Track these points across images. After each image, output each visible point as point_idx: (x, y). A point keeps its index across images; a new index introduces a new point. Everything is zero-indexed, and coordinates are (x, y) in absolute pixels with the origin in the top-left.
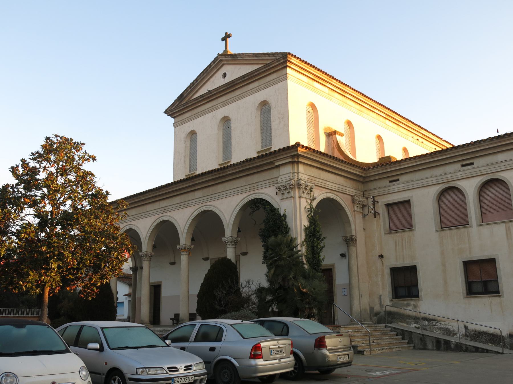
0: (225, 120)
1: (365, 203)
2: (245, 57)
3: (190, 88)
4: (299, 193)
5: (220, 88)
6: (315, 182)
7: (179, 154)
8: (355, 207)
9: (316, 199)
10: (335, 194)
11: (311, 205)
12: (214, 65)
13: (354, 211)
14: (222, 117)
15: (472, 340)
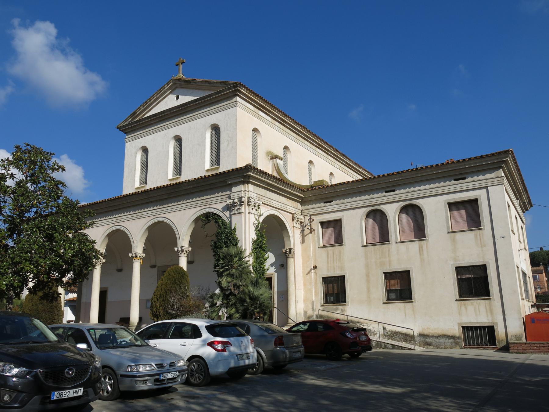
1: (303, 221)
4: (249, 210)
6: (262, 200)
8: (295, 223)
9: (263, 215)
10: (278, 211)
11: (258, 220)
12: (168, 87)
13: (294, 227)
15: (389, 339)
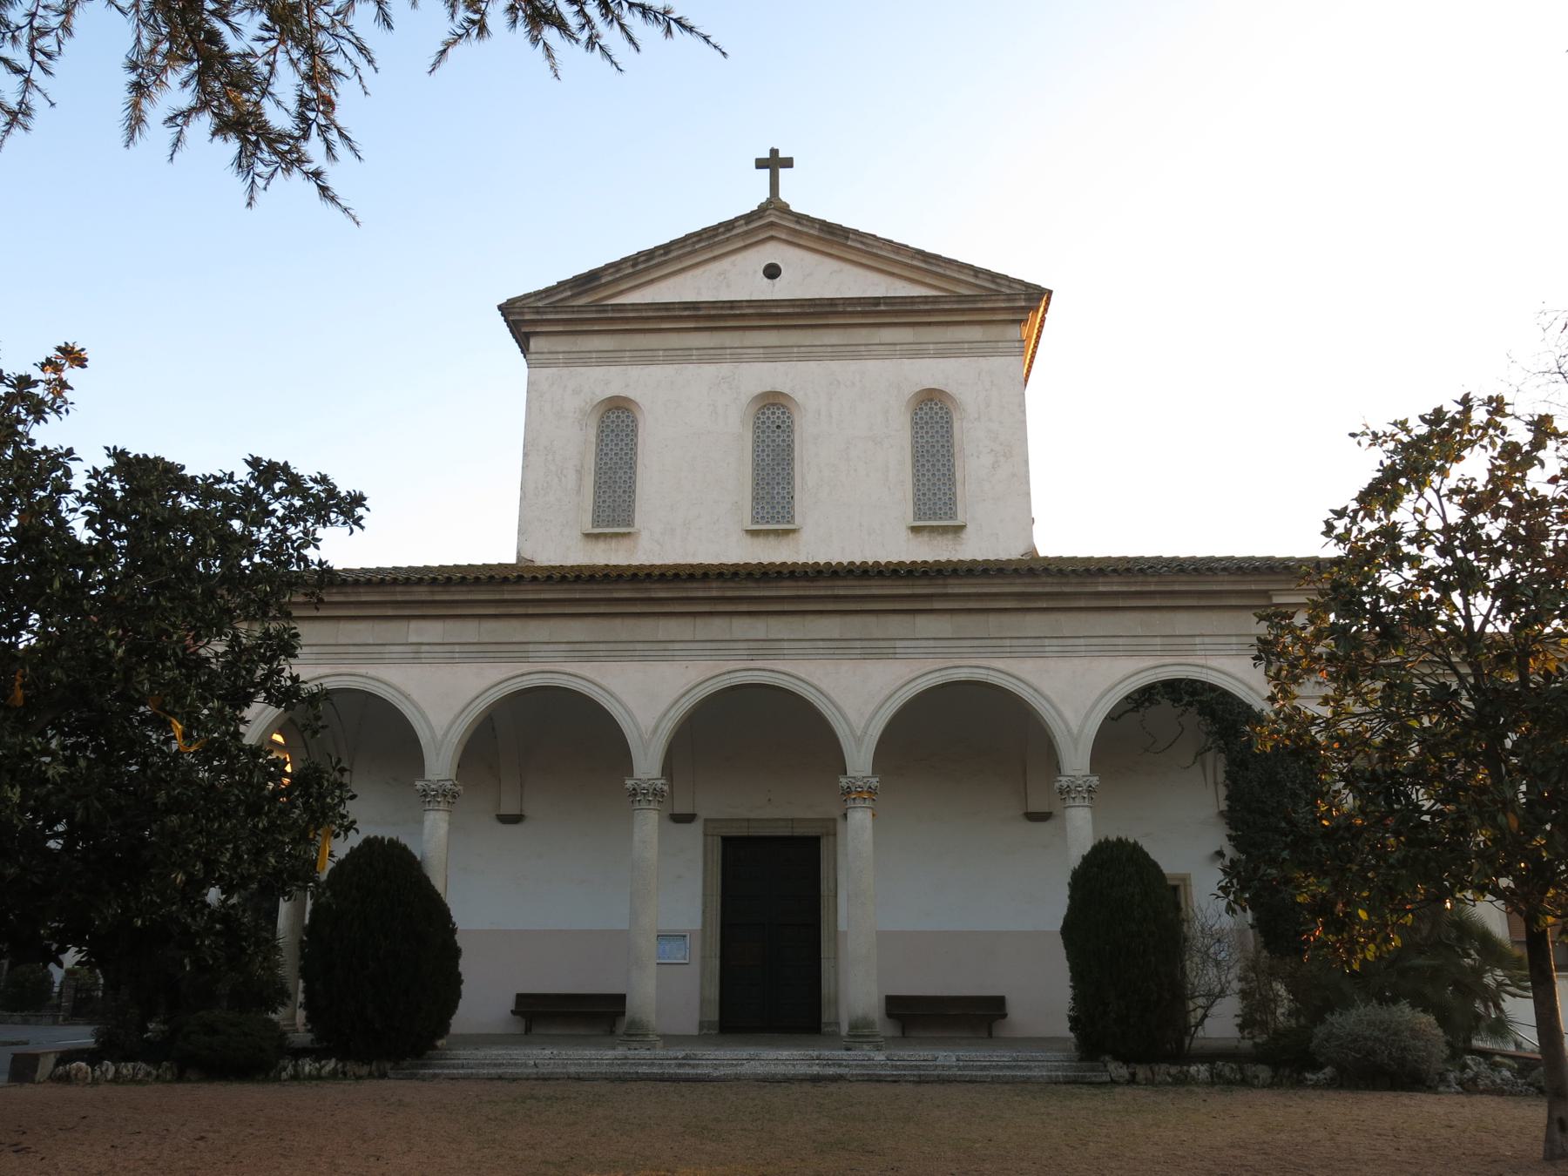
0: (766, 402)
2: (881, 248)
3: (634, 266)
5: (775, 304)
7: (550, 458)
14: (760, 390)
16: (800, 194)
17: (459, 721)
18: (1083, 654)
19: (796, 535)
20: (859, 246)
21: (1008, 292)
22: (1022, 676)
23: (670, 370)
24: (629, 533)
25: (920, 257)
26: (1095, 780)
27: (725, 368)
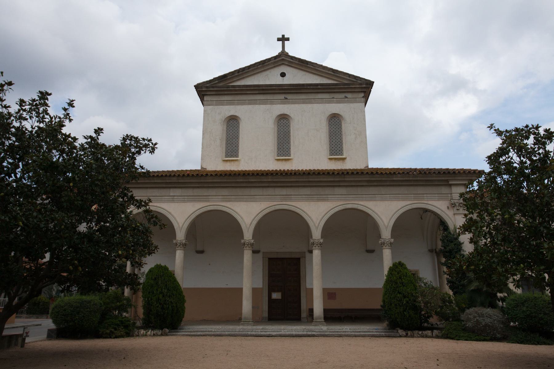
2: (318, 68)
3: (238, 73)
16: (292, 50)
17: (187, 221)
18: (388, 200)
19: (291, 161)
20: (312, 67)
21: (360, 82)
22: (369, 207)
23: (250, 107)
24: (237, 160)
25: (331, 70)
26: (392, 240)
27: (268, 106)
